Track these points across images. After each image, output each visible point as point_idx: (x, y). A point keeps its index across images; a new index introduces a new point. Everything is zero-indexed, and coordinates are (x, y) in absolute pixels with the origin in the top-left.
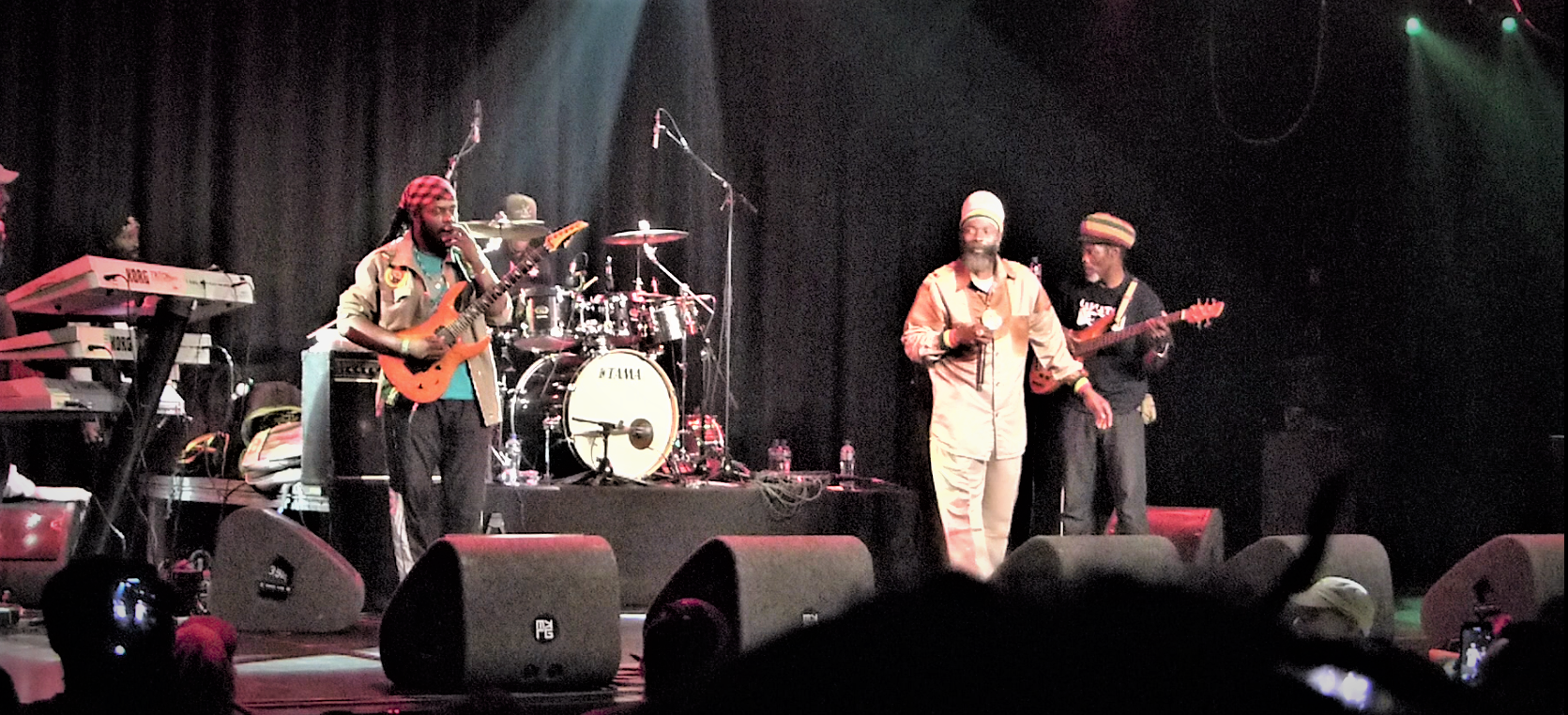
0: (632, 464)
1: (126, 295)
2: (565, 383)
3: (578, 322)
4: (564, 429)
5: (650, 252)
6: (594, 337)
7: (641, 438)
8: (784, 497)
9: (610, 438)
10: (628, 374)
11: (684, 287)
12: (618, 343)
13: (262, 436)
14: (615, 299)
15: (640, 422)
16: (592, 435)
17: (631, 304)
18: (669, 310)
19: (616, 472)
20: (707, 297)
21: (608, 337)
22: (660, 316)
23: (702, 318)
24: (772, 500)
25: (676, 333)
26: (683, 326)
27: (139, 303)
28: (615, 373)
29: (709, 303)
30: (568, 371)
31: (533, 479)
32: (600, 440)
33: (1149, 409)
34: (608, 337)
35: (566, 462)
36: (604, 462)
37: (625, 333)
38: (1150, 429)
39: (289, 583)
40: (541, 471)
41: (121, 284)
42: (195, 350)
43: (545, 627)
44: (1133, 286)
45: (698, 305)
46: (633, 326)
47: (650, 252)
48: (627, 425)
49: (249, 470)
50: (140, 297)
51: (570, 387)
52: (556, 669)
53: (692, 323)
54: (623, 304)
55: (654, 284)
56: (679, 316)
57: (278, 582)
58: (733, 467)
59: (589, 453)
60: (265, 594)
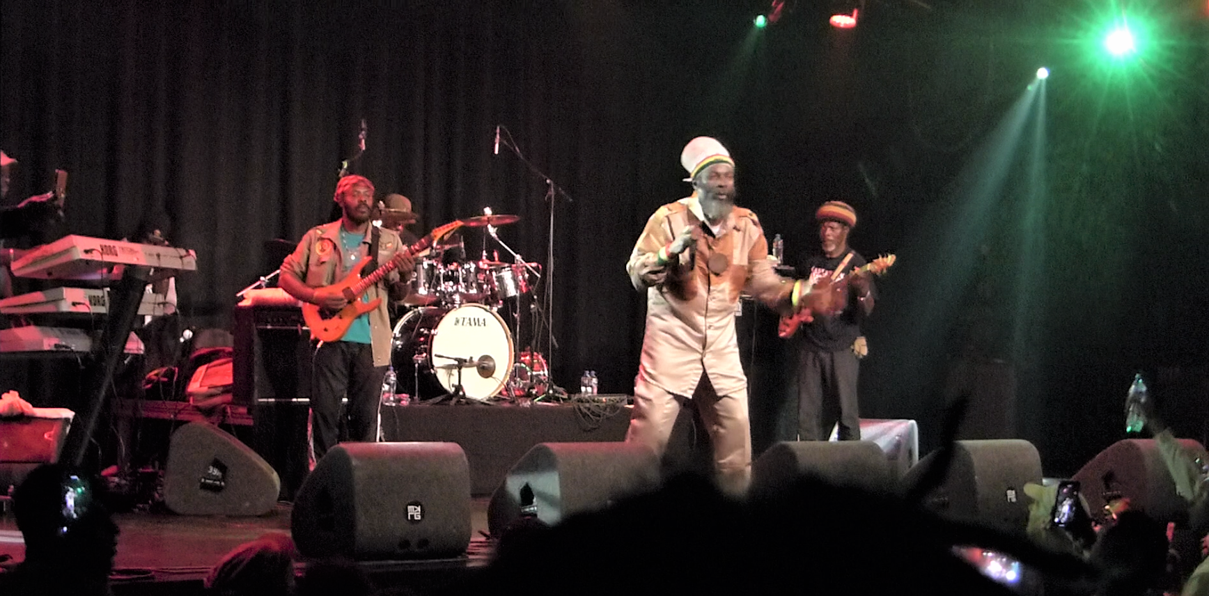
0: (479, 389)
1: (101, 265)
2: (430, 329)
3: (438, 284)
4: (428, 364)
5: (492, 231)
6: (451, 294)
7: (486, 370)
8: (593, 413)
9: (464, 370)
10: (476, 322)
11: (518, 257)
12: (469, 299)
13: (202, 370)
14: (466, 266)
15: (486, 358)
16: (449, 368)
17: (478, 270)
18: (507, 275)
19: (468, 395)
20: (534, 265)
21: (462, 294)
22: (500, 279)
23: (531, 280)
24: (585, 415)
25: (512, 291)
26: (517, 287)
27: (110, 270)
28: (467, 321)
29: (537, 269)
30: (432, 321)
31: (406, 400)
32: (455, 372)
33: (861, 347)
34: (462, 294)
35: (430, 386)
36: (459, 388)
37: (474, 291)
38: (864, 363)
39: (223, 478)
40: (412, 396)
41: (96, 257)
42: (151, 307)
43: (414, 511)
44: (850, 256)
46: (480, 287)
47: (492, 231)
48: (476, 360)
49: (191, 394)
50: (110, 266)
51: (433, 332)
52: (424, 543)
53: (522, 284)
54: (472, 270)
55: (496, 254)
57: (216, 478)
58: (555, 392)
59: (447, 381)
60: (205, 487)
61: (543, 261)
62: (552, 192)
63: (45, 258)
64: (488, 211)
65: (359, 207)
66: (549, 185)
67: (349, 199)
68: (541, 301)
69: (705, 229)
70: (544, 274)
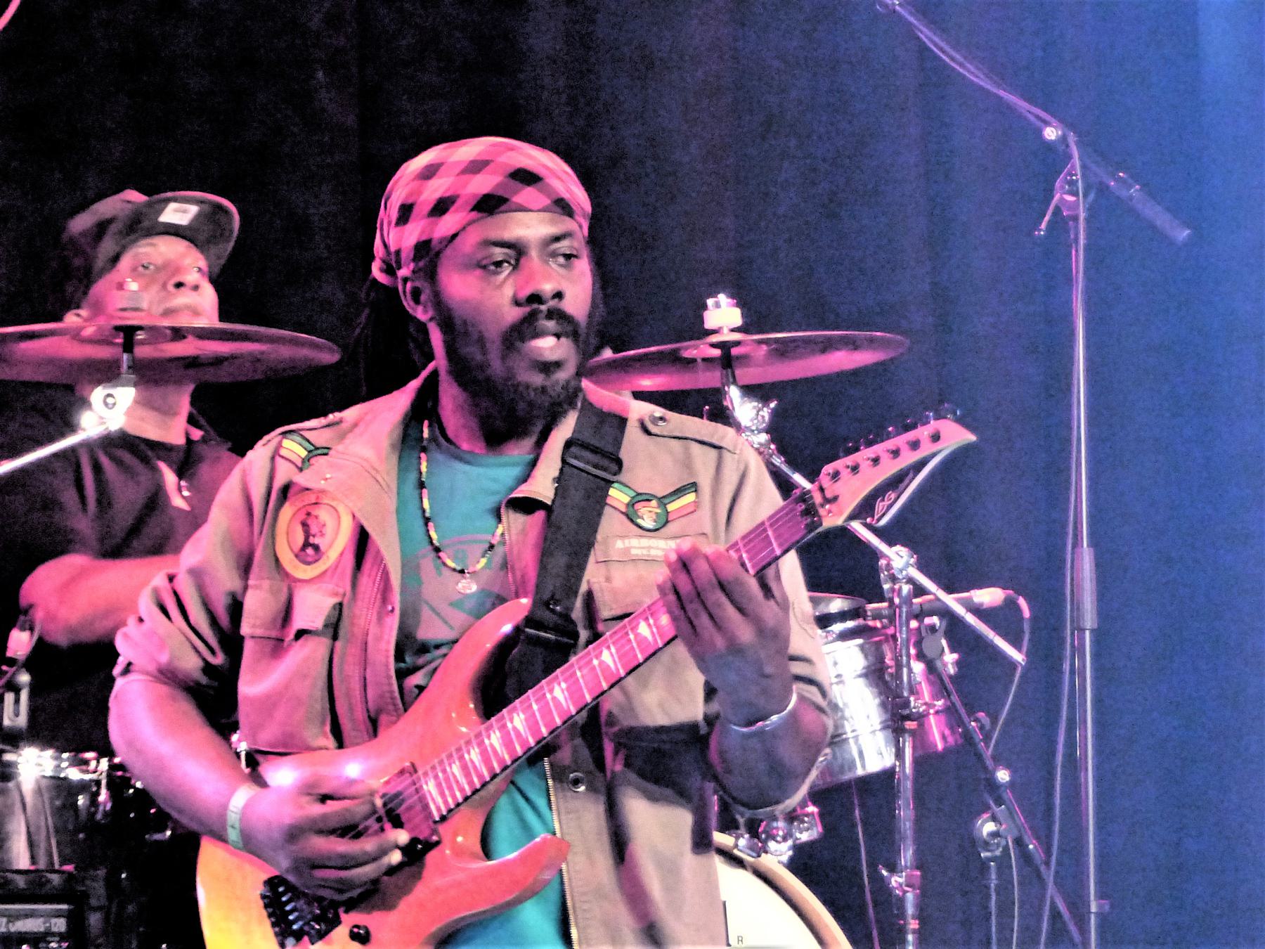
20: (989, 596)
23: (977, 675)
25: (871, 749)
26: (898, 718)
45: (956, 630)
53: (924, 700)
56: (877, 674)
61: (1043, 581)
62: (1069, 197)
63: (1077, 543)
64: (723, 315)
65: (524, 329)
66: (1053, 158)
67: (460, 286)
68: (1036, 799)
69: (740, 245)
70: (1048, 644)
